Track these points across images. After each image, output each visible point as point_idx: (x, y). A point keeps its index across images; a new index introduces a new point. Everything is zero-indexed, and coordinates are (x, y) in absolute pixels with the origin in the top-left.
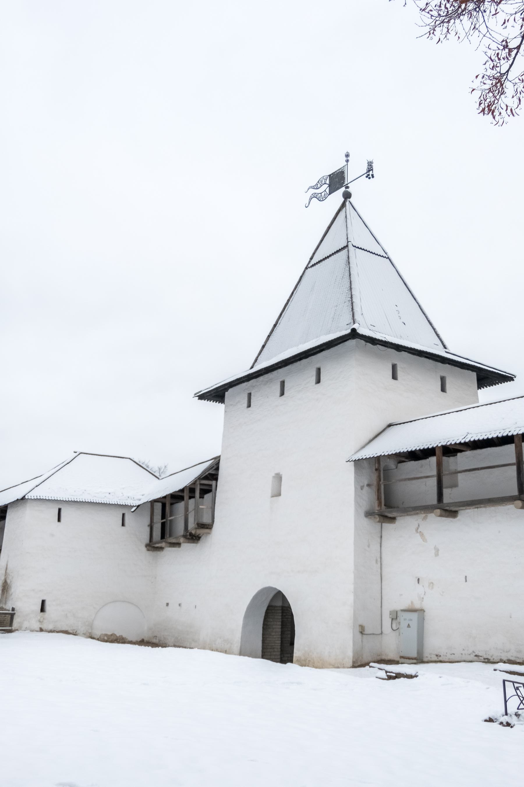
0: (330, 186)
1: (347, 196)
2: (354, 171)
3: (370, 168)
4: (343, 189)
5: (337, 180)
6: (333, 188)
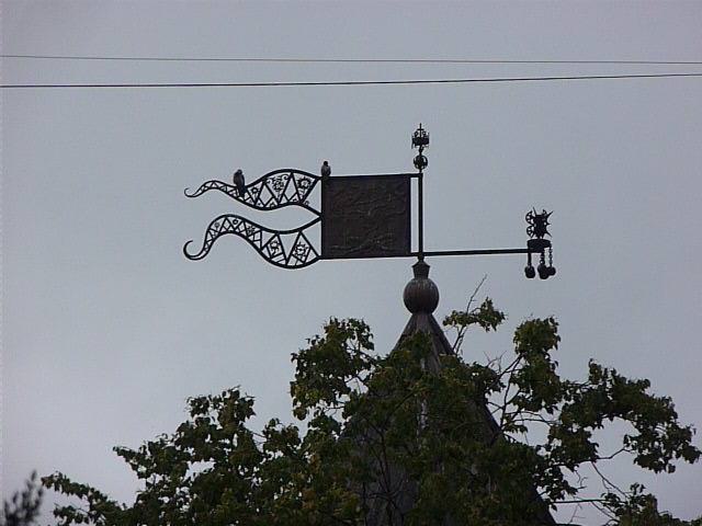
3: (538, 246)
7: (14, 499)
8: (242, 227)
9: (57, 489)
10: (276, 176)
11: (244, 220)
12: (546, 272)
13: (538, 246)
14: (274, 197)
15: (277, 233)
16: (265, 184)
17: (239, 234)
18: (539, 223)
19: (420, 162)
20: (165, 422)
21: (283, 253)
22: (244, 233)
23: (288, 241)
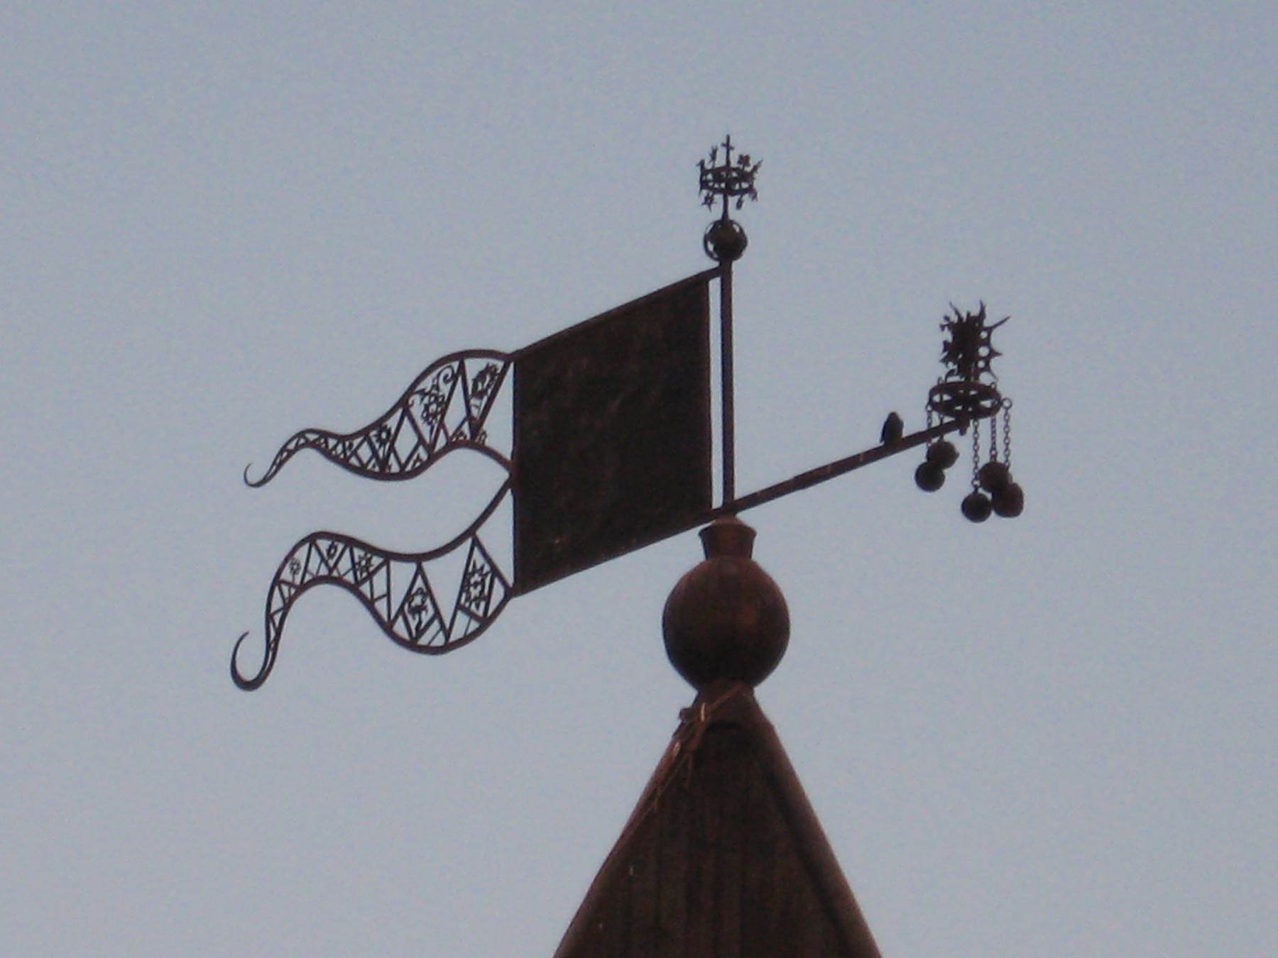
0: (529, 478)
1: (727, 632)
2: (796, 387)
3: (966, 394)
4: (681, 553)
5: (613, 428)
6: (562, 526)
7: (713, 157)
8: (345, 564)
9: (929, 477)
10: (427, 384)
11: (351, 542)
12: (997, 495)
13: (966, 394)
14: (421, 440)
15: (418, 559)
16: (407, 413)
17: (339, 581)
18: (967, 339)
19: (726, 243)
20: (942, 348)
21: (437, 614)
22: (350, 578)
23: (445, 578)
